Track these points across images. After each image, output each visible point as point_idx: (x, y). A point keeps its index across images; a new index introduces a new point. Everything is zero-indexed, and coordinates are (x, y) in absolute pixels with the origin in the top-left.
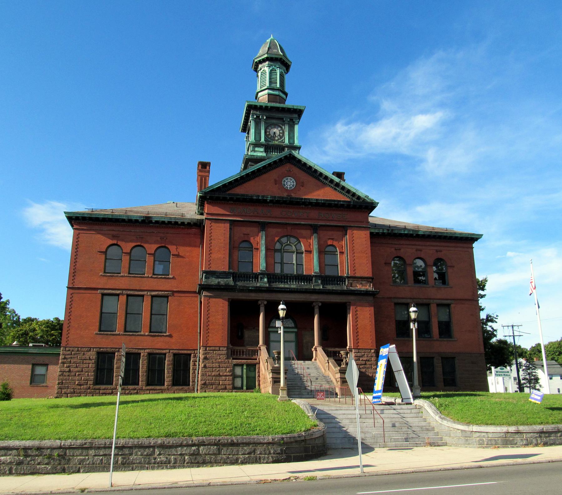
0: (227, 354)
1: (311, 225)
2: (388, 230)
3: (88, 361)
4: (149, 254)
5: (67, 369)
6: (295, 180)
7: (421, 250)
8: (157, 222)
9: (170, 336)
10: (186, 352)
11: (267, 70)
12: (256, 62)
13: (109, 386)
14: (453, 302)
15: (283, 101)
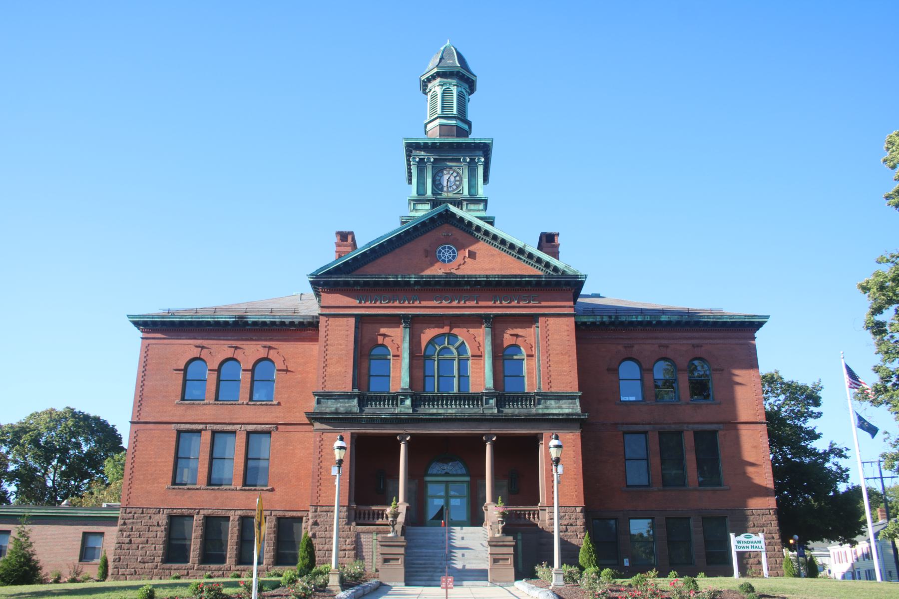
0: (348, 517)
1: (405, 317)
2: (610, 317)
3: (155, 528)
4: (210, 370)
5: (127, 540)
7: (667, 347)
8: (255, 323)
9: (272, 490)
10: (294, 514)
11: (439, 91)
13: (183, 565)
14: (721, 426)
15: (462, 133)
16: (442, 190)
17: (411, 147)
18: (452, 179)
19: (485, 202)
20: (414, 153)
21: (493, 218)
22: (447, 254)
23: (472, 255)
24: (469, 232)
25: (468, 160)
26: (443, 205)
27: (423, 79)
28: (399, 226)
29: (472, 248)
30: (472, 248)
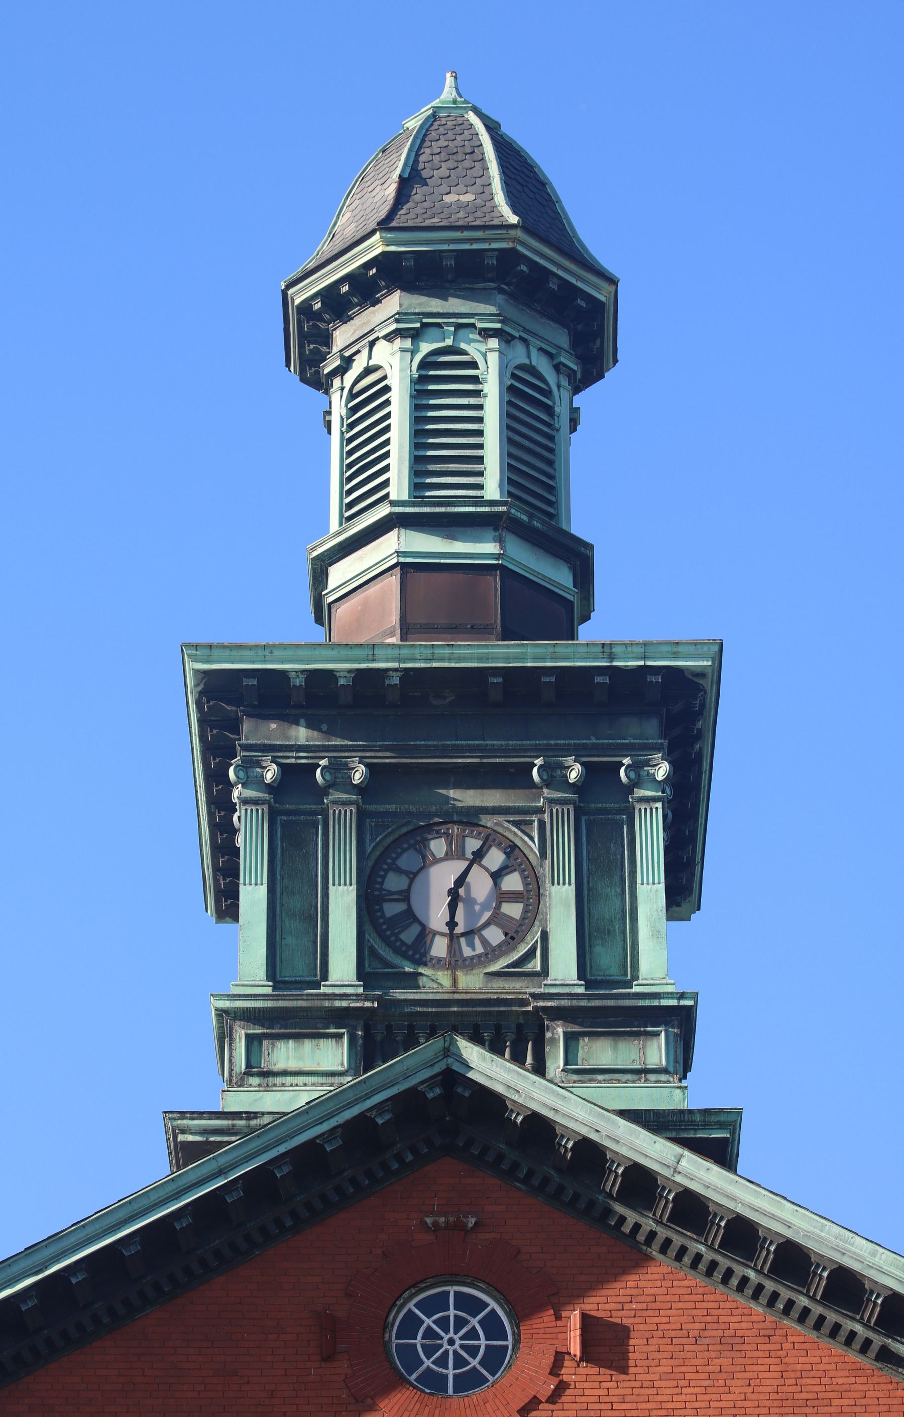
6: (417, 1286)
11: (394, 363)
12: (305, 308)
15: (556, 613)
16: (418, 952)
17: (232, 702)
18: (480, 885)
19: (680, 1020)
20: (251, 731)
21: (730, 1120)
22: (452, 1342)
23: (606, 1345)
24: (587, 1207)
25: (574, 774)
26: (428, 1048)
27: (299, 295)
28: (156, 1167)
29: (607, 1302)
30: (604, 1303)
